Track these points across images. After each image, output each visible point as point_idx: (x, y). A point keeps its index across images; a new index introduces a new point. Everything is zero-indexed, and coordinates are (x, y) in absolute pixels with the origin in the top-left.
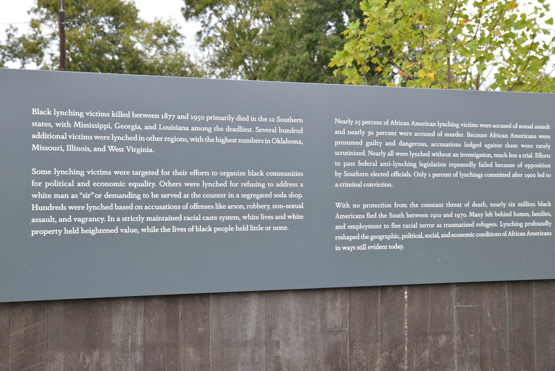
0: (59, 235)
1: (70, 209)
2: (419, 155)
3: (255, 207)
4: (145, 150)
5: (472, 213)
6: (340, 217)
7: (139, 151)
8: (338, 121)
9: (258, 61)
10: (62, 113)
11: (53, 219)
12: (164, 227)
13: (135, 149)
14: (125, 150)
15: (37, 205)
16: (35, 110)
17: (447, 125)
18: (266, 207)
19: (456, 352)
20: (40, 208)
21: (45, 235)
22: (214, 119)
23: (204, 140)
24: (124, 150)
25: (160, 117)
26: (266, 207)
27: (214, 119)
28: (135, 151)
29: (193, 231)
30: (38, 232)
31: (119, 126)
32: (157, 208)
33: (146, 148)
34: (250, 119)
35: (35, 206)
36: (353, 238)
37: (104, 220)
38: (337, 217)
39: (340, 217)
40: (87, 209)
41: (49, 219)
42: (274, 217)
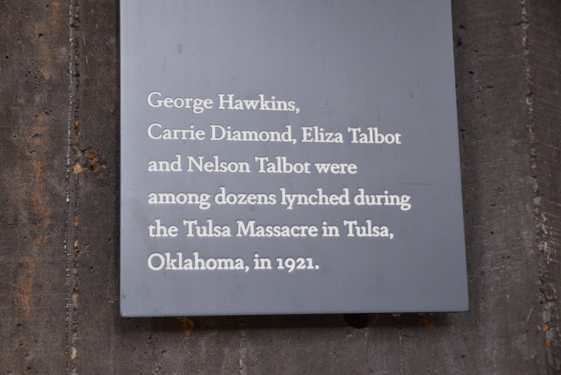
1: (320, 171)
2: (314, 200)
9: (507, 296)
10: (303, 200)
12: (158, 222)
15: (231, 96)
17: (314, 200)
19: (555, 203)
22: (387, 203)
27: (387, 203)
30: (346, 169)
35: (226, 98)
40: (284, 203)
41: (204, 228)
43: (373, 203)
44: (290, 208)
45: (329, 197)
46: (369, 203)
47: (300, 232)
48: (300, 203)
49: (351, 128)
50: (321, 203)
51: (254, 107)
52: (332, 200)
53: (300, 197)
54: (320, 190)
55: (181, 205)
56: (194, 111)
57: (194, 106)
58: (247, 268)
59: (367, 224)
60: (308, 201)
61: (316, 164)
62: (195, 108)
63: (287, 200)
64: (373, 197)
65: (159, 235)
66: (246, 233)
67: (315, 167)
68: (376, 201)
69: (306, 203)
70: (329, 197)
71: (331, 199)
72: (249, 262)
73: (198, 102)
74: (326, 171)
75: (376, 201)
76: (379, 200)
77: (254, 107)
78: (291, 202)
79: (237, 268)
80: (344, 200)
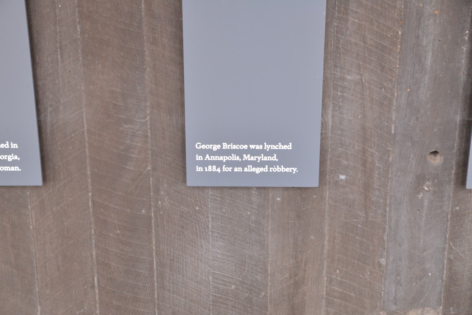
1: (251, 148)
3: (279, 170)
5: (247, 156)
6: (210, 158)
7: (258, 170)
8: (17, 169)
10: (273, 147)
16: (225, 145)
18: (292, 170)
21: (224, 161)
25: (204, 169)
26: (292, 170)
31: (200, 146)
34: (10, 146)
36: (228, 158)
37: (297, 170)
38: (207, 159)
39: (210, 158)
40: (265, 148)
42: (243, 169)
48: (272, 148)
49: (205, 158)
50: (280, 148)
53: (272, 146)
55: (241, 149)
58: (240, 160)
59: (248, 167)
60: (275, 147)
63: (267, 147)
66: (246, 159)
67: (250, 147)
69: (274, 148)
72: (242, 157)
74: (254, 148)
78: (268, 148)
80: (289, 147)
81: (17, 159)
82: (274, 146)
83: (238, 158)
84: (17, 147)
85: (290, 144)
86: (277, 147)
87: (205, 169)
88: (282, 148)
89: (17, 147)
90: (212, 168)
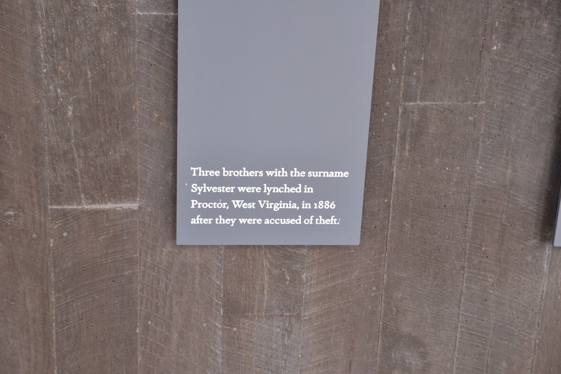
0: (232, 225)
2: (282, 190)
4: (286, 206)
10: (276, 190)
11: (335, 220)
13: (271, 204)
14: (257, 205)
20: (315, 174)
23: (289, 174)
24: (255, 206)
25: (313, 206)
28: (271, 207)
29: (311, 223)
32: (283, 222)
33: (288, 203)
40: (265, 191)
43: (317, 176)
44: (268, 194)
45: (249, 172)
46: (314, 176)
47: (213, 205)
48: (274, 191)
50: (285, 191)
51: (272, 175)
52: (292, 190)
53: (274, 188)
54: (285, 185)
56: (274, 210)
57: (274, 207)
58: (298, 208)
60: (279, 190)
61: (238, 188)
62: (275, 208)
63: (267, 190)
64: (317, 172)
65: (283, 175)
68: (318, 175)
69: (277, 192)
70: (249, 172)
71: (291, 189)
72: (299, 205)
73: (276, 205)
75: (318, 175)
76: (320, 174)
77: (272, 175)
78: (269, 191)
79: (330, 176)
81: (295, 207)
82: (277, 188)
83: (295, 206)
84: (312, 192)
85: (193, 207)
86: (282, 190)
87: (314, 206)
88: (248, 175)
89: (312, 192)
90: (324, 204)
